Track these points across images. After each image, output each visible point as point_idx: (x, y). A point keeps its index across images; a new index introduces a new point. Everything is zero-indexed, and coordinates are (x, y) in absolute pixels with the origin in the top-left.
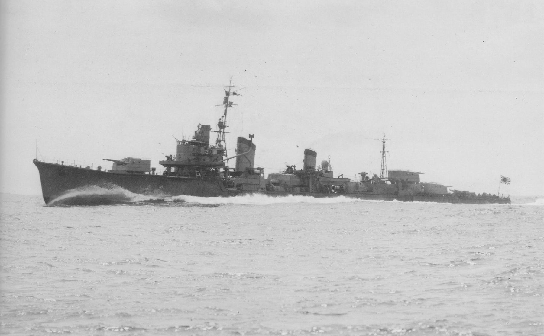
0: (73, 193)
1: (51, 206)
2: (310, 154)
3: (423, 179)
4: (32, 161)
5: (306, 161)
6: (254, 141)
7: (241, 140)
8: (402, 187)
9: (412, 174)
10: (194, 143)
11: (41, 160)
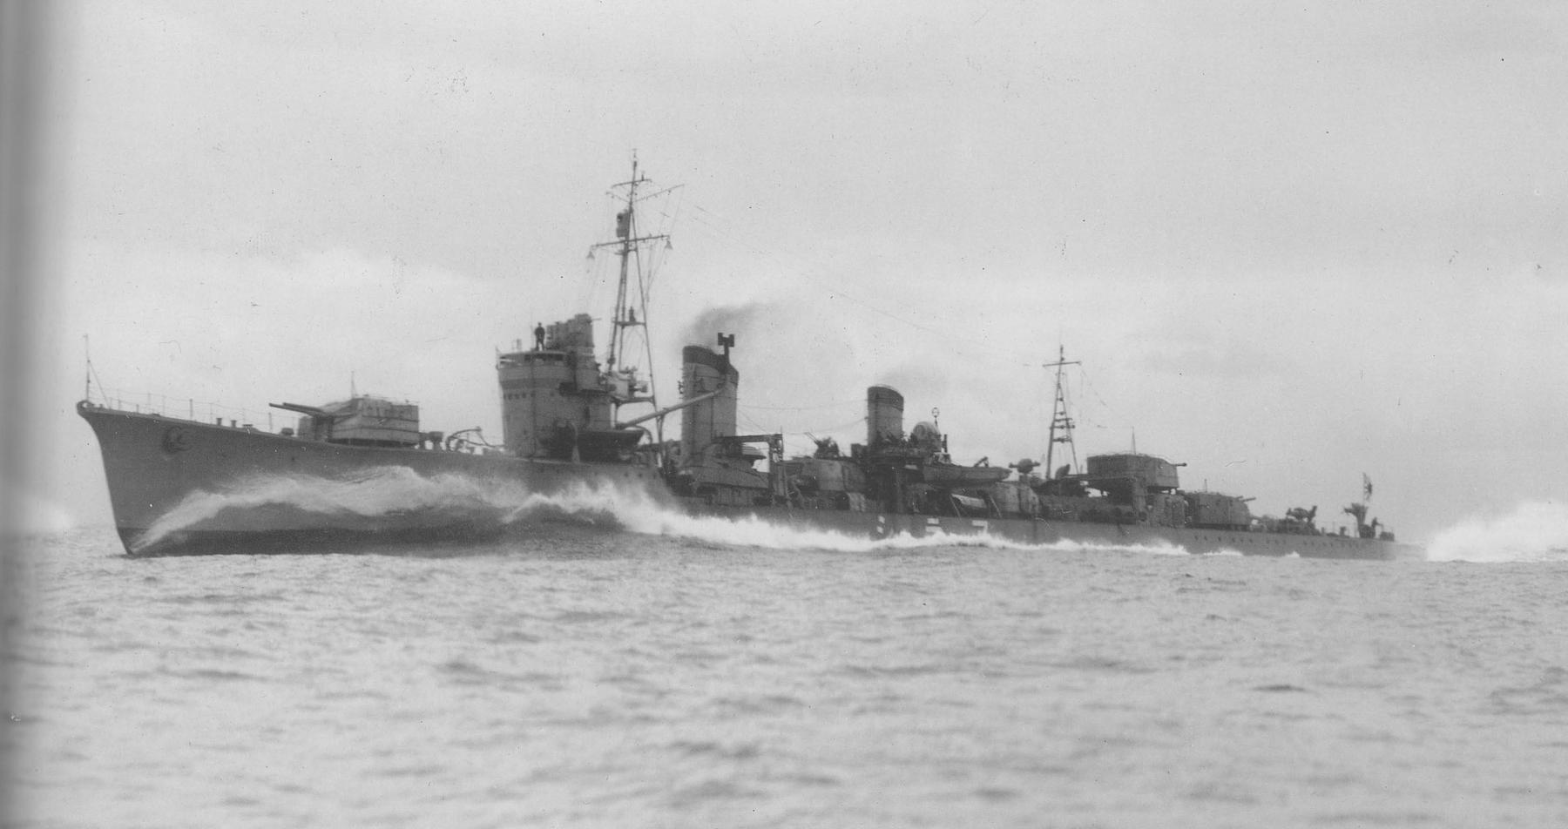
0: (199, 507)
1: (172, 547)
2: (884, 400)
3: (1189, 482)
4: (74, 410)
5: (874, 420)
6: (736, 359)
7: (693, 355)
8: (1120, 497)
9: (1229, 501)
10: (541, 356)
11: (97, 401)
